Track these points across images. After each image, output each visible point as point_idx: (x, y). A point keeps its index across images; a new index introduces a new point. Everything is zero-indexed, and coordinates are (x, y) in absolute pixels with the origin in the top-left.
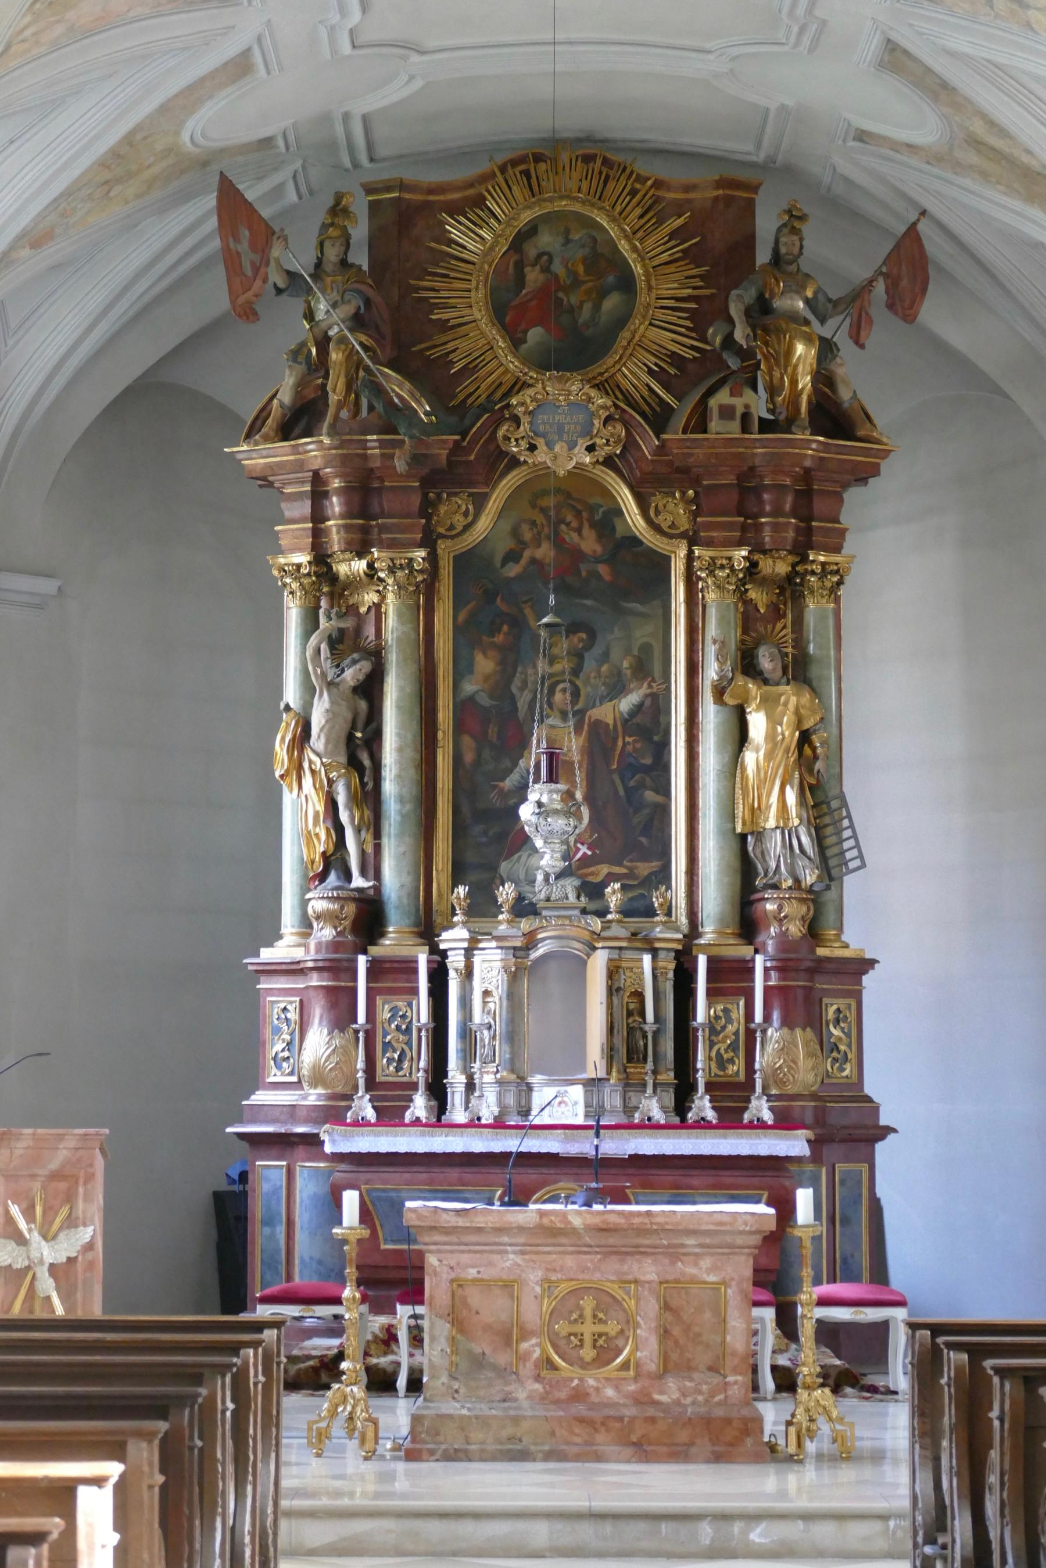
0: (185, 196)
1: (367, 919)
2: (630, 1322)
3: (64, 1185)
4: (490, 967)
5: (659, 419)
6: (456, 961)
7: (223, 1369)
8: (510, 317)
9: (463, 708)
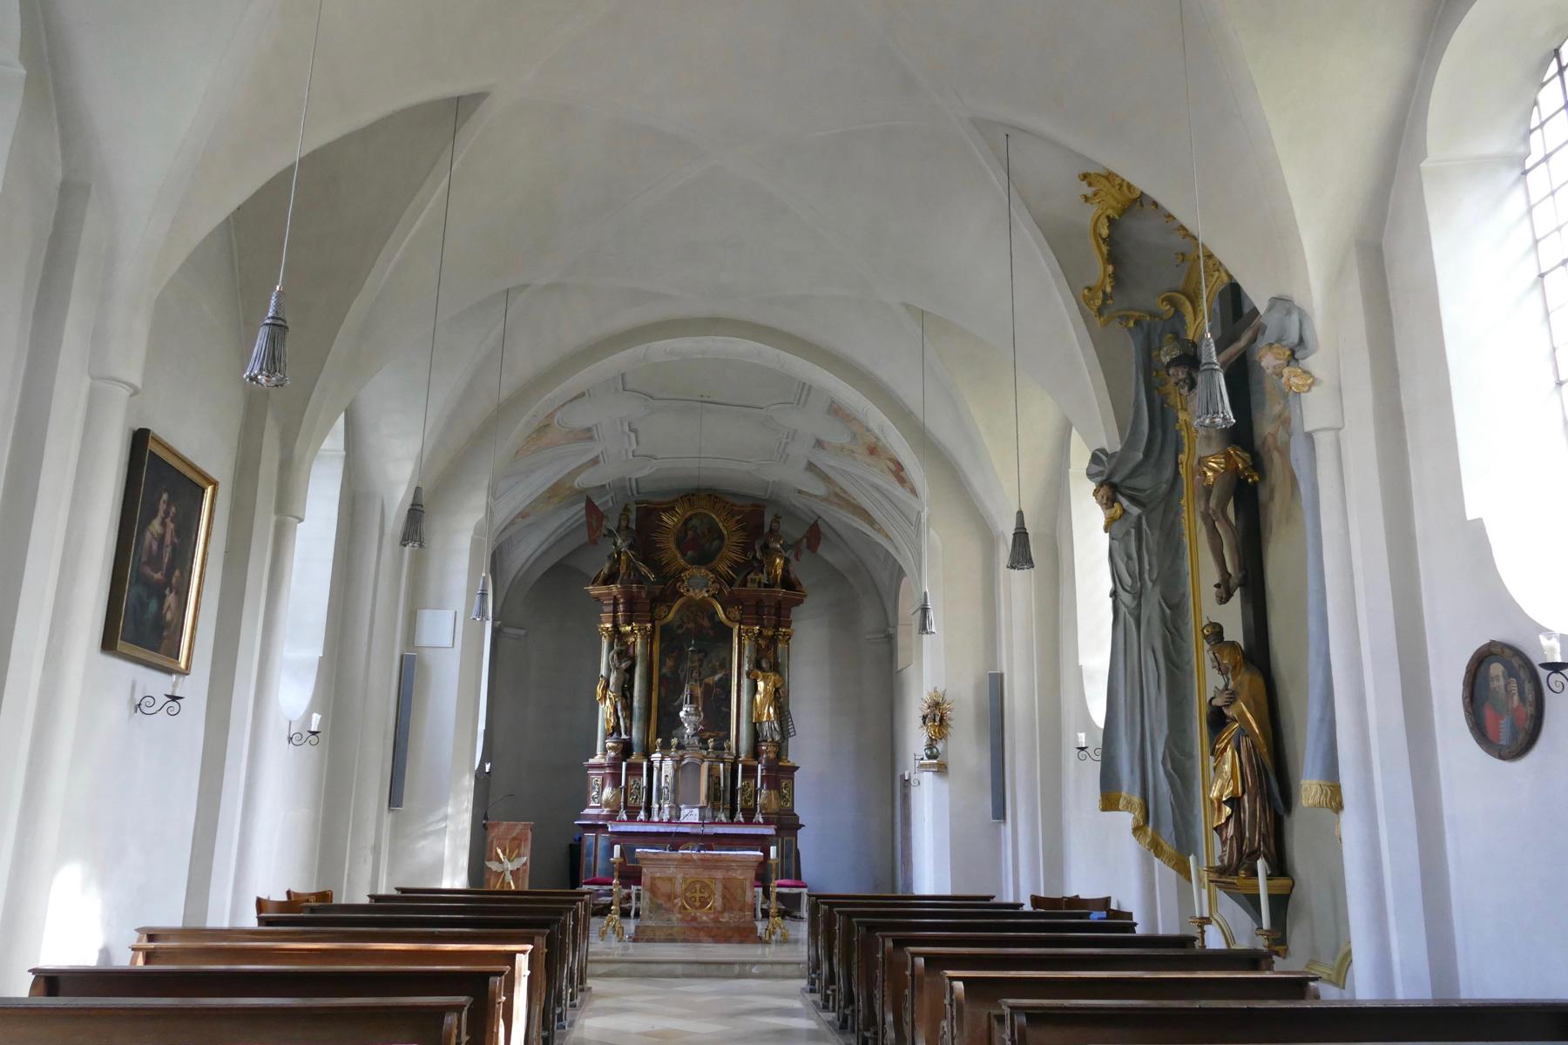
0: (573, 504)
1: (626, 749)
2: (712, 893)
3: (517, 842)
4: (668, 766)
5: (731, 582)
6: (656, 764)
7: (569, 910)
8: (682, 545)
9: (662, 678)
